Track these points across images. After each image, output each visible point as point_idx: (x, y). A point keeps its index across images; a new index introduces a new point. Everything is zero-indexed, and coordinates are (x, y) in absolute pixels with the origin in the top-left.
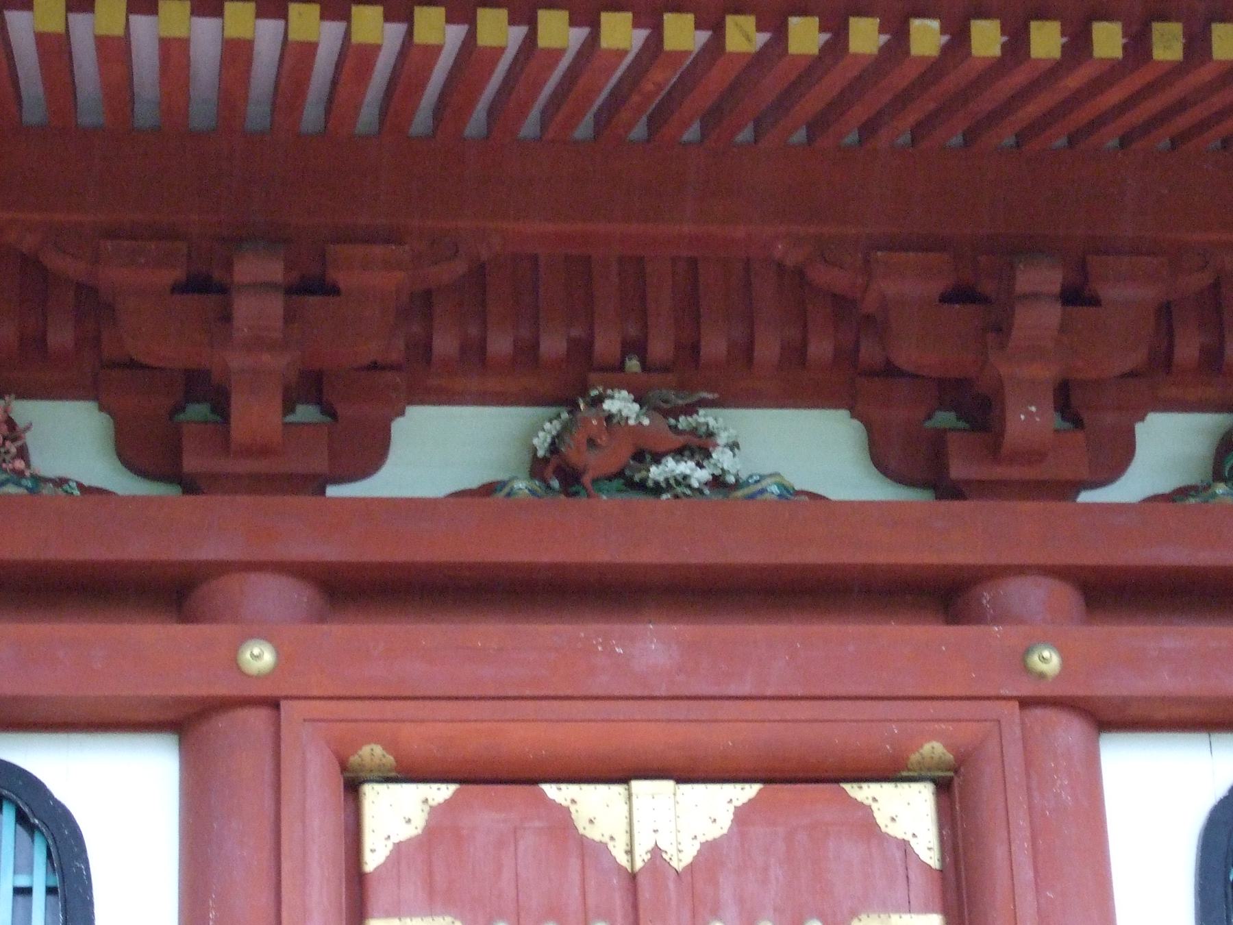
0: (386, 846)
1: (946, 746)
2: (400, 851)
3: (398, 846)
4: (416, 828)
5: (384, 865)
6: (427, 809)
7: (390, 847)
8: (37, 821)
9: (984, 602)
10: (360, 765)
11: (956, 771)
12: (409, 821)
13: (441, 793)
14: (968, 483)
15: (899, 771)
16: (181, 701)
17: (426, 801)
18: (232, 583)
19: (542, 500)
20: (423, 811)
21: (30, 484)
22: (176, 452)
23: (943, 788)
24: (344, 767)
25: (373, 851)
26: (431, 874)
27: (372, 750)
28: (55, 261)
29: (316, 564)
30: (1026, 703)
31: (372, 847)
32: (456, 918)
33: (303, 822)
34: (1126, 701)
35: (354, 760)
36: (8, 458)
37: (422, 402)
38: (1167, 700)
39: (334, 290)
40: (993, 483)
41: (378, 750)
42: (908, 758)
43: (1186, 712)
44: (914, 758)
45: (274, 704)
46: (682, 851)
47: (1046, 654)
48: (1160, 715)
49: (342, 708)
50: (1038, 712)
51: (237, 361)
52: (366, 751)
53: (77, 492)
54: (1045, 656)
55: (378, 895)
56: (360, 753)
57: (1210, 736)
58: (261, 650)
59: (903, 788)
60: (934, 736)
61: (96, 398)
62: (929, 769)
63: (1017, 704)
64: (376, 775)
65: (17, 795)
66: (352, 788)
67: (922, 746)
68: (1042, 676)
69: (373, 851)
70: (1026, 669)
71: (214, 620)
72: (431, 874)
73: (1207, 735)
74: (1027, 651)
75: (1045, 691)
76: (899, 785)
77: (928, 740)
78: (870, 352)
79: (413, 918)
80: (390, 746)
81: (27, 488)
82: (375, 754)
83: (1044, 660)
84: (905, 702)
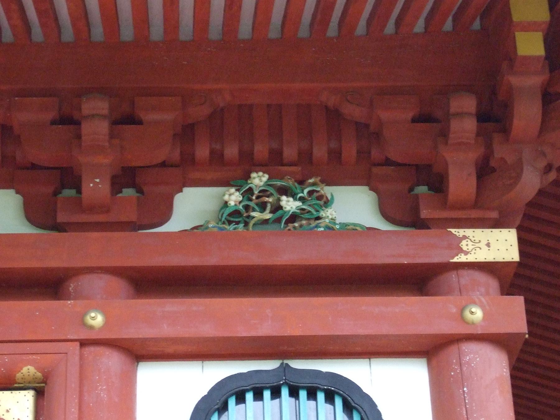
1: (36, 368)
9: (70, 289)
10: (22, 378)
11: (45, 383)
12: (8, 411)
14: (69, 224)
15: (14, 384)
19: (223, 231)
22: (416, 210)
23: (40, 394)
30: (84, 343)
34: (144, 341)
37: (191, 186)
38: (175, 341)
40: (83, 223)
42: (15, 376)
43: (181, 348)
44: (19, 376)
47: (93, 315)
48: (170, 350)
50: (92, 349)
52: (25, 370)
53: (366, 230)
54: (473, 311)
56: (22, 371)
57: (370, 360)
58: (95, 314)
59: (16, 393)
60: (29, 363)
61: (367, 184)
62: (29, 383)
63: (78, 344)
67: (22, 369)
68: (91, 327)
70: (84, 324)
73: (368, 360)
74: (85, 313)
75: (93, 336)
76: (13, 392)
77: (26, 365)
78: (375, 154)
83: (472, 313)
84: (15, 344)
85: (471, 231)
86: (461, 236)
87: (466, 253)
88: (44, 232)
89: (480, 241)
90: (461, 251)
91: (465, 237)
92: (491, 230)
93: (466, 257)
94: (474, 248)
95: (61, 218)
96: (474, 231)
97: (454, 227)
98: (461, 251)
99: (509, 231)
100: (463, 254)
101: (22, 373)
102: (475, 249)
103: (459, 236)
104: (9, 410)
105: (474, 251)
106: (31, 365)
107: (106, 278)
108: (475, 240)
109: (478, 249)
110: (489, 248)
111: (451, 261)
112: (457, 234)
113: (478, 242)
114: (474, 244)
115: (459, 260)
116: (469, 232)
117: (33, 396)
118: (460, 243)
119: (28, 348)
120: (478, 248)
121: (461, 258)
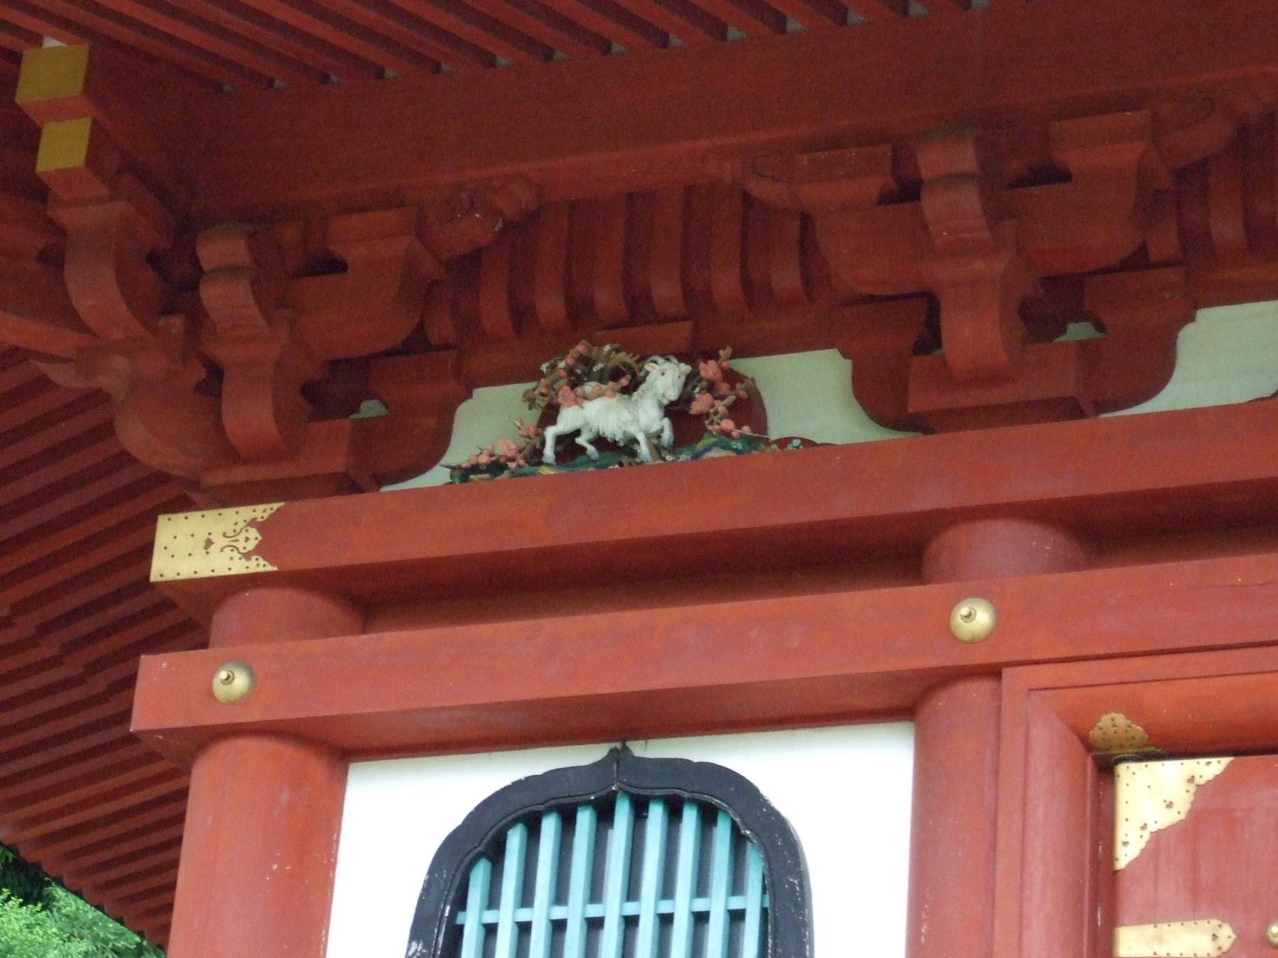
0: (1141, 836)
2: (1159, 842)
3: (1157, 835)
4: (1179, 813)
5: (1136, 860)
6: (1193, 788)
7: (1147, 836)
8: (748, 832)
13: (1210, 768)
16: (897, 679)
17: (1191, 780)
18: (954, 536)
20: (1187, 791)
21: (739, 446)
24: (1088, 746)
25: (1125, 843)
26: (1195, 867)
27: (1113, 720)
28: (762, 189)
29: (1060, 503)
31: (1125, 839)
32: (1224, 921)
33: (1024, 811)
35: (1095, 733)
36: (716, 419)
39: (1064, 176)
41: (1120, 719)
45: (993, 672)
46: (1145, 824)
49: (1075, 672)
51: (941, 274)
52: (1105, 721)
55: (1132, 896)
56: (1100, 724)
64: (1131, 751)
65: (721, 800)
66: (1106, 769)
69: (1125, 843)
71: (941, 579)
72: (1195, 867)
77: (1107, 712)
79: (1172, 924)
80: (1134, 713)
81: (736, 450)
82: (1117, 724)
85: (242, 570)
86: (254, 557)
87: (253, 523)
88: (896, 437)
89: (222, 551)
90: (261, 526)
91: (247, 556)
92: (164, 579)
93: (253, 515)
94: (239, 534)
95: (917, 403)
96: (213, 571)
97: (273, 572)
98: (261, 526)
99: (178, 574)
100: (260, 520)
101: (1100, 729)
102: (235, 533)
103: (257, 557)
104: (1168, 803)
105: (238, 528)
106: (1116, 712)
107: (272, 746)
108: (232, 550)
109: (230, 533)
110: (210, 537)
111: (282, 504)
112: (262, 562)
113: (225, 550)
114: (234, 544)
115: (268, 506)
116: (239, 567)
117: (1117, 860)
118: (261, 541)
119: (733, 792)
120: (229, 535)
121: (262, 511)
